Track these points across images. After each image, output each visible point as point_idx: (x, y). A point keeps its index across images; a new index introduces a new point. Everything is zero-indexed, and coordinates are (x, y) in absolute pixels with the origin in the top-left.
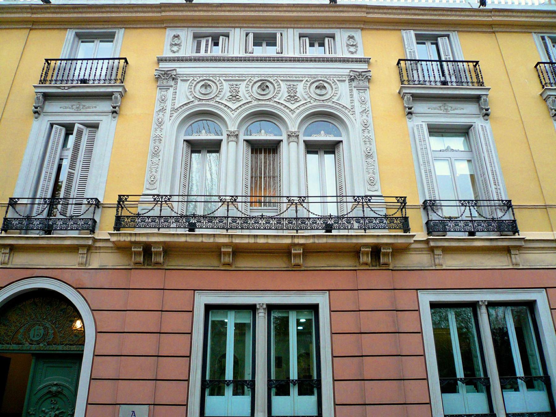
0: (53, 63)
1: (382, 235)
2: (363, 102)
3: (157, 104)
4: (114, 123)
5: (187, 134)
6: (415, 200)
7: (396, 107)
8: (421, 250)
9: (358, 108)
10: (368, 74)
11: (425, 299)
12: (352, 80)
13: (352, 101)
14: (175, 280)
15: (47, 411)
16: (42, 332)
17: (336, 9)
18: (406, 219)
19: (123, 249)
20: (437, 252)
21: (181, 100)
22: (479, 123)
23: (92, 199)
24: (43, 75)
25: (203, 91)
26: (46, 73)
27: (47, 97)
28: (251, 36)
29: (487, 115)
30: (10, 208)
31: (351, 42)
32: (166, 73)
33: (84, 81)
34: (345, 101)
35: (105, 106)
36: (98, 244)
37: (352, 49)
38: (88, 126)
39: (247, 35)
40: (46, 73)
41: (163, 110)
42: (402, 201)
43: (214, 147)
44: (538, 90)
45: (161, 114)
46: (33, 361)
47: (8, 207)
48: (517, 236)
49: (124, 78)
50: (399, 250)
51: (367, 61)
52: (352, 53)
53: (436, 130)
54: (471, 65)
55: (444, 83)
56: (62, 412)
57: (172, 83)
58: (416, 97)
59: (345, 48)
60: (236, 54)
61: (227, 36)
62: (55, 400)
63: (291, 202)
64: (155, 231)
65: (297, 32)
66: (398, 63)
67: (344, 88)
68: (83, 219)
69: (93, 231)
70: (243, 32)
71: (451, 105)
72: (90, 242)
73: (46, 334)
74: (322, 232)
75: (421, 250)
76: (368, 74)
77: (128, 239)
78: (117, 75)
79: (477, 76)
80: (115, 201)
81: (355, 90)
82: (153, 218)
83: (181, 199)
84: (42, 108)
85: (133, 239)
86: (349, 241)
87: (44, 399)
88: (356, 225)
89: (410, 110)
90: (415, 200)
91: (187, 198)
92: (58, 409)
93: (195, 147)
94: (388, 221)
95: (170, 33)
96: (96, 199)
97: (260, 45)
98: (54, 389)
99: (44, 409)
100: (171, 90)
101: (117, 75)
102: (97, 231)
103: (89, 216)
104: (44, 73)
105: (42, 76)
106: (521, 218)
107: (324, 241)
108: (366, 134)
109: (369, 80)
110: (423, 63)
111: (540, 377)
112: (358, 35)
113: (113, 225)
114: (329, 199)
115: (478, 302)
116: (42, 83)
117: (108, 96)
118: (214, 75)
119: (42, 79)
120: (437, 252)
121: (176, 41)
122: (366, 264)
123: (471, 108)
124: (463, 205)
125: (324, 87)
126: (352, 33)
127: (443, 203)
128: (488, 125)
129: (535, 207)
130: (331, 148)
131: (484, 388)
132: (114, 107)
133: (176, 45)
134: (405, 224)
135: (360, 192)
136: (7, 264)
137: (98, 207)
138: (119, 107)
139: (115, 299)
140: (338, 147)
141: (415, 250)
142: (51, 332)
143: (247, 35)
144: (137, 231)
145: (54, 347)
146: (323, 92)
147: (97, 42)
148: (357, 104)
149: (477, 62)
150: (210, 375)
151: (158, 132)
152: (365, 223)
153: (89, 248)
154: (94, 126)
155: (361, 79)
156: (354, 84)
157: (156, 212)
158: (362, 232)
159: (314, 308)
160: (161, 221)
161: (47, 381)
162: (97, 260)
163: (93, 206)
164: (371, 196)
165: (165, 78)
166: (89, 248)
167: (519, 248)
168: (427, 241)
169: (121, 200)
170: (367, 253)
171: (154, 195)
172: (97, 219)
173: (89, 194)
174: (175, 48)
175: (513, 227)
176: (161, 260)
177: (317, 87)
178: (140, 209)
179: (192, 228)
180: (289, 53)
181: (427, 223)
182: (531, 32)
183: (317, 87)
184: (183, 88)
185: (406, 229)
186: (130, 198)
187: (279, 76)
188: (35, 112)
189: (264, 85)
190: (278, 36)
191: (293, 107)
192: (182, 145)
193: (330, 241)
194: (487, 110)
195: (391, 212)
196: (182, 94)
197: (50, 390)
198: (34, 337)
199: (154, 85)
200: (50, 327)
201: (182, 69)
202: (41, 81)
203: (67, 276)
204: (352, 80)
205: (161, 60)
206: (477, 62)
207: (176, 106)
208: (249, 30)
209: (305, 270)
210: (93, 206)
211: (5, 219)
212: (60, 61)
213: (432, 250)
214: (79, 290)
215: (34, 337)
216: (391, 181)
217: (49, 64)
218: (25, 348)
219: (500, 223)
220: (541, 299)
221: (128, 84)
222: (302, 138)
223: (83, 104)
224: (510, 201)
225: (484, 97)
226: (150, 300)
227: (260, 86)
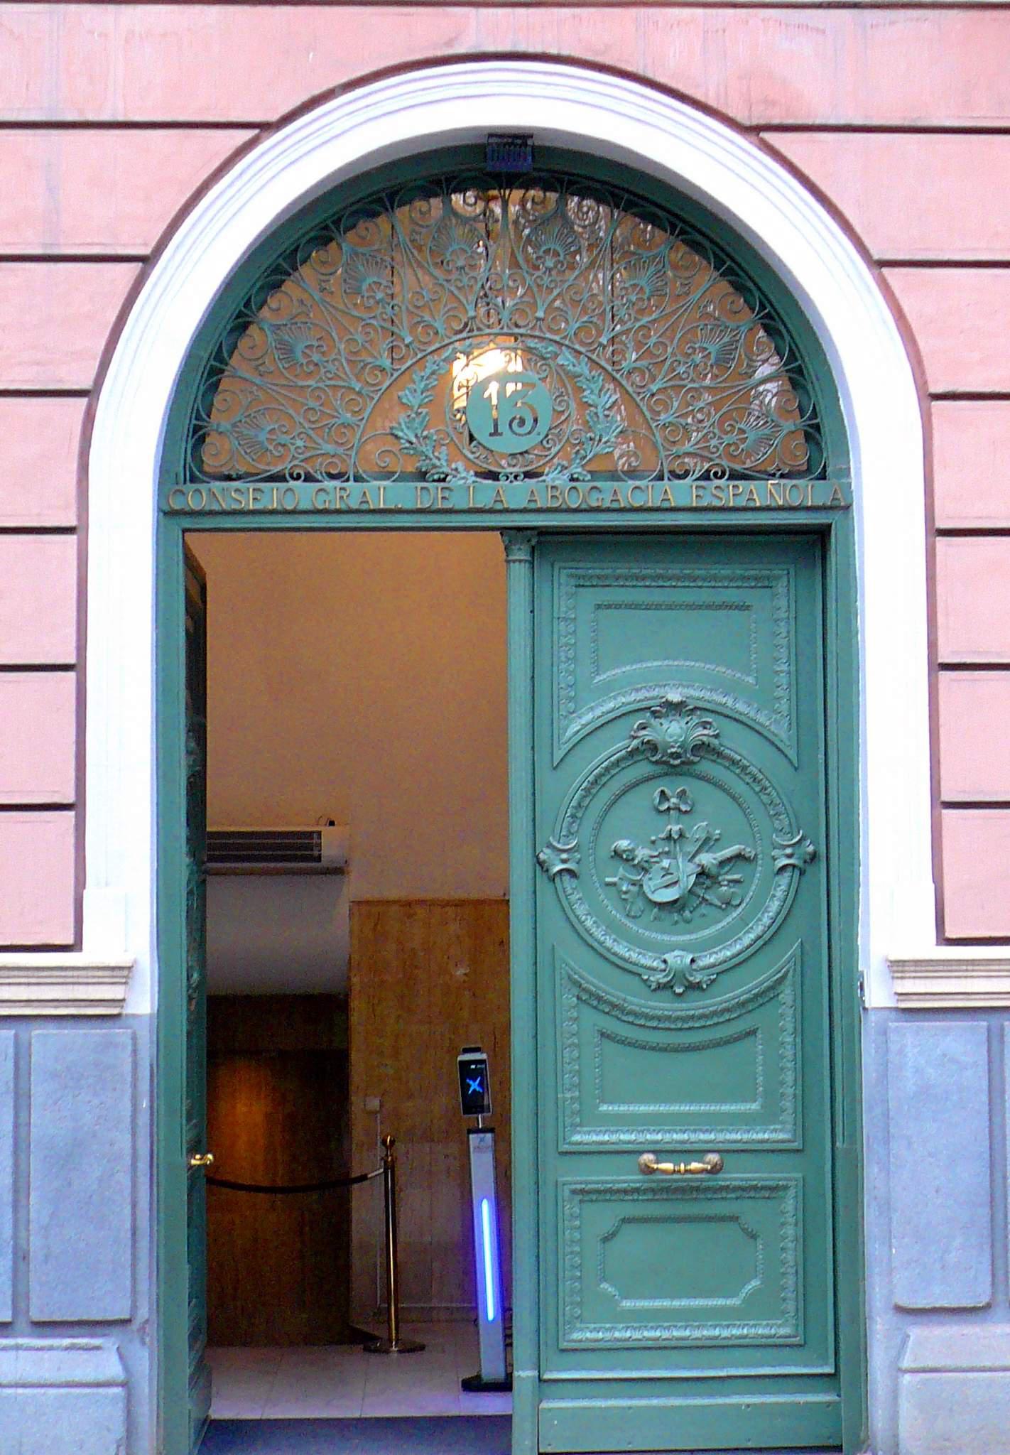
15: (642, 853)
46: (520, 572)
56: (739, 857)
62: (682, 795)
87: (616, 785)
92: (707, 843)
98: (673, 731)
99: (624, 844)
145: (627, 493)
150: (550, 1410)
161: (607, 689)
197: (647, 735)
198: (496, 433)
200: (583, 368)
209: (240, 209)
214: (768, 136)
215: (496, 433)
218: (456, 502)
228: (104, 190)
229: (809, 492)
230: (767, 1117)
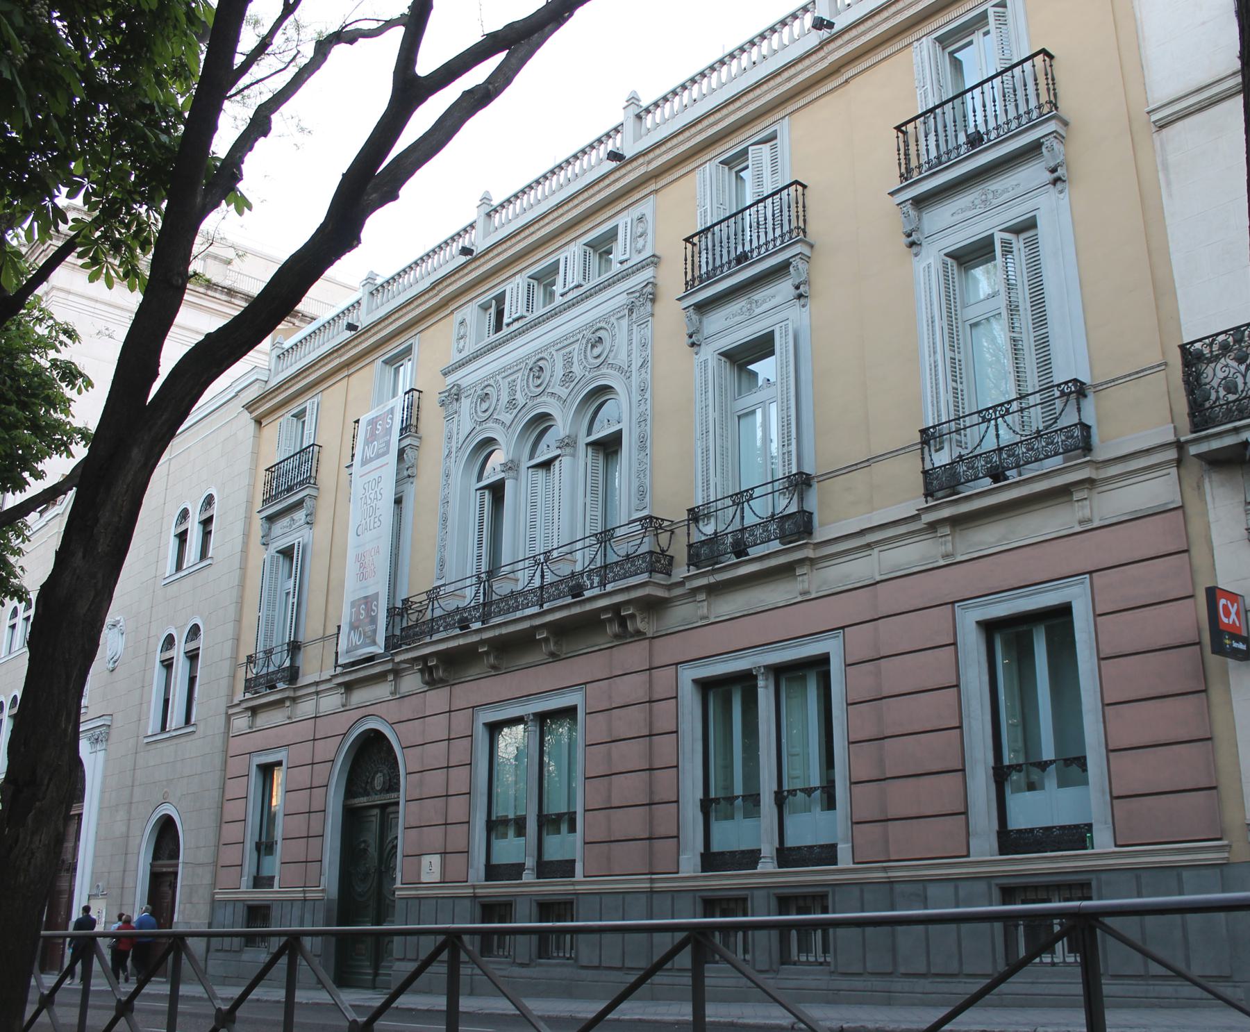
0: (910, 127)
4: (1064, 199)
11: (969, 618)
23: (1066, 383)
24: (903, 161)
26: (907, 155)
27: (920, 202)
30: (692, 526)
33: (742, 258)
35: (1033, 173)
38: (1017, 230)
40: (907, 155)
47: (922, 449)
49: (1055, 95)
50: (654, 606)
68: (1061, 430)
69: (1087, 448)
71: (759, 295)
78: (1038, 95)
89: (1056, 175)
96: (1075, 381)
101: (1038, 95)
103: (1069, 418)
104: (902, 156)
105: (900, 164)
107: (461, 642)
115: (750, 670)
116: (906, 179)
119: (903, 170)
124: (984, 420)
132: (1053, 170)
136: (1090, 520)
137: (1085, 396)
138: (805, 283)
141: (405, 669)
153: (294, 700)
154: (1027, 226)
163: (1073, 396)
167: (811, 562)
172: (1089, 418)
173: (1060, 375)
182: (911, 43)
188: (693, 345)
202: (901, 175)
210: (1073, 396)
212: (1029, 63)
217: (905, 133)
222: (583, 440)
223: (993, 188)
228: (932, 626)
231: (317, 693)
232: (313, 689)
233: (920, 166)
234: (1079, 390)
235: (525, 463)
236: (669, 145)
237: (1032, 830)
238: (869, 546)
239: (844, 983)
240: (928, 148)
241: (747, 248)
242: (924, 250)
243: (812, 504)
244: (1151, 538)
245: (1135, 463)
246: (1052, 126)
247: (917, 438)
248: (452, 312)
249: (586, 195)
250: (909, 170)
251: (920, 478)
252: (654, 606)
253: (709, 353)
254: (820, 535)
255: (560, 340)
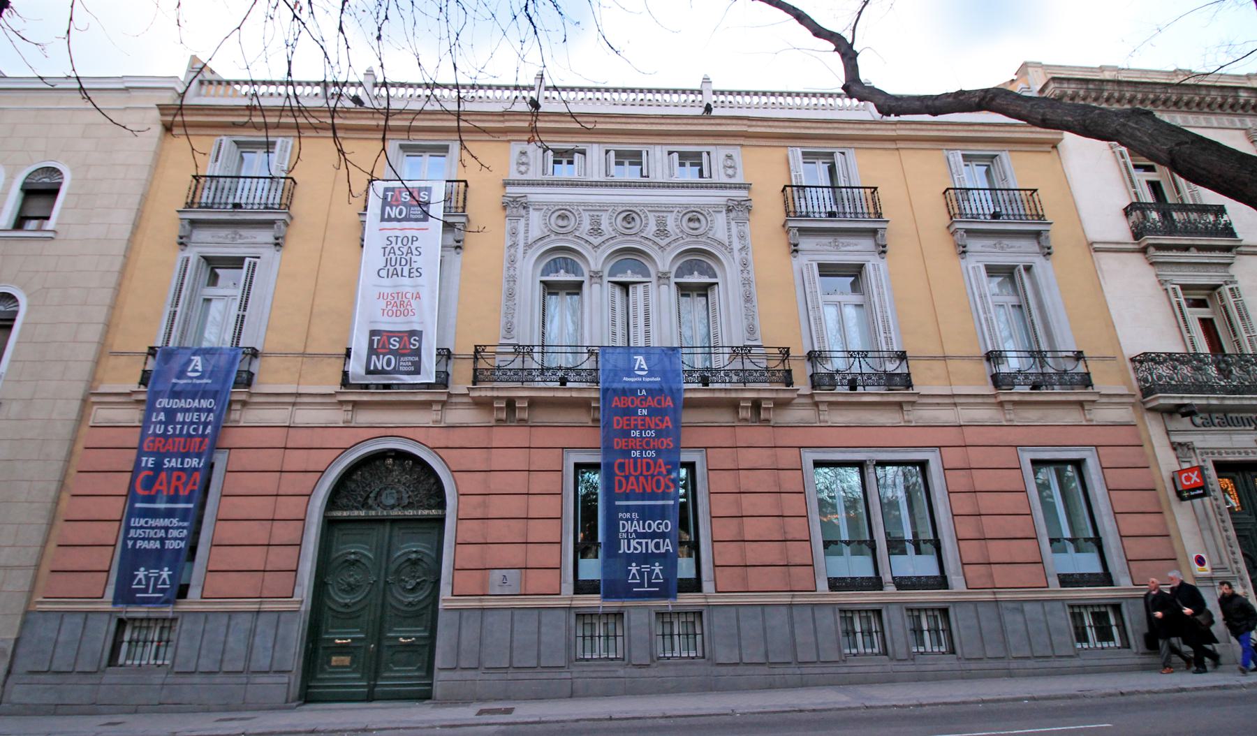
1: (765, 391)
2: (742, 237)
3: (507, 237)
5: (542, 275)
6: (800, 349)
7: (780, 245)
8: (803, 405)
9: (736, 245)
10: (748, 203)
11: (1026, 457)
12: (729, 210)
13: (730, 236)
14: (541, 437)
16: (395, 495)
17: (712, 121)
18: (789, 372)
19: (483, 404)
20: (821, 407)
21: (535, 233)
22: (1039, 262)
25: (561, 223)
27: (194, 223)
28: (612, 154)
29: (884, 252)
31: (729, 163)
32: (515, 200)
33: (237, 206)
34: (721, 234)
35: (266, 236)
36: (454, 400)
37: (730, 172)
39: (607, 152)
41: (514, 245)
42: (786, 353)
43: (575, 288)
44: (947, 221)
45: (513, 250)
48: (1090, 389)
51: (746, 187)
52: (730, 176)
53: (827, 270)
54: (868, 191)
55: (995, 216)
57: (523, 212)
58: (803, 231)
59: (722, 171)
60: (596, 178)
61: (583, 153)
63: (591, 353)
64: (519, 385)
65: (398, 143)
66: (784, 190)
67: (721, 219)
69: (446, 386)
70: (603, 148)
71: (1006, 242)
72: (444, 398)
73: (400, 499)
74: (700, 386)
75: (803, 405)
76: (748, 203)
77: (489, 394)
79: (875, 204)
80: (472, 351)
81: (733, 223)
82: (516, 371)
83: (721, 350)
84: (188, 237)
85: (495, 394)
86: (728, 395)
88: (735, 378)
90: (800, 349)
91: (710, 349)
93: (550, 288)
94: (767, 374)
95: (516, 148)
97: (622, 164)
98: (414, 556)
100: (523, 221)
102: (450, 385)
106: (1094, 368)
108: (745, 275)
109: (749, 211)
110: (813, 190)
111: (865, 541)
112: (736, 152)
113: (138, 379)
114: (695, 350)
117: (270, 224)
118: (571, 204)
120: (1007, 407)
121: (524, 159)
122: (746, 420)
123: (866, 243)
125: (698, 220)
126: (729, 151)
127: (833, 354)
128: (883, 264)
129: (934, 358)
130: (704, 290)
131: (869, 551)
132: (277, 239)
133: (523, 164)
134: (788, 379)
135: (738, 342)
139: (475, 459)
140: (713, 290)
142: (405, 495)
143: (607, 152)
144: (495, 385)
146: (696, 225)
147: (426, 157)
148: (735, 240)
149: (876, 188)
151: (511, 272)
152: (745, 377)
155: (740, 209)
156: (732, 215)
157: (517, 364)
158: (741, 386)
159: (923, 465)
160: (524, 376)
162: (457, 416)
164: (751, 347)
165: (515, 206)
166: (444, 404)
167: (913, 403)
168: (812, 396)
169: (478, 352)
170: (747, 407)
171: (514, 345)
174: (523, 168)
175: (907, 382)
176: (525, 415)
177: (690, 220)
178: (498, 361)
179: (563, 381)
180: (658, 175)
181: (812, 376)
183: (690, 220)
184: (535, 217)
185: (789, 383)
186: (488, 349)
187: (645, 205)
188: (181, 244)
189: (629, 218)
190: (644, 154)
191: (663, 243)
192: (539, 289)
193: (567, 394)
194: (884, 246)
195: (772, 364)
196: (536, 224)
199: (503, 214)
201: (536, 195)
203: (419, 435)
204: (729, 210)
205: (507, 184)
206: (876, 188)
207: (530, 241)
208: (608, 147)
211: (144, 371)
213: (816, 404)
216: (778, 329)
219: (890, 376)
220: (932, 457)
221: (297, 207)
224: (1081, 352)
225: (880, 232)
226: (516, 459)
227: (625, 218)
229: (440, 512)
230: (424, 631)
231: (294, 404)
232: (291, 400)
233: (226, 204)
234: (254, 353)
235: (673, 280)
236: (771, 123)
237: (844, 578)
238: (955, 404)
239: (973, 666)
240: (205, 196)
241: (243, 201)
242: (188, 249)
243: (256, 367)
244: (1123, 436)
245: (1112, 399)
246: (283, 217)
247: (146, 350)
248: (509, 141)
249: (690, 121)
250: (192, 202)
251: (140, 373)
252: (782, 404)
253: (193, 253)
254: (255, 388)
255: (659, 205)
